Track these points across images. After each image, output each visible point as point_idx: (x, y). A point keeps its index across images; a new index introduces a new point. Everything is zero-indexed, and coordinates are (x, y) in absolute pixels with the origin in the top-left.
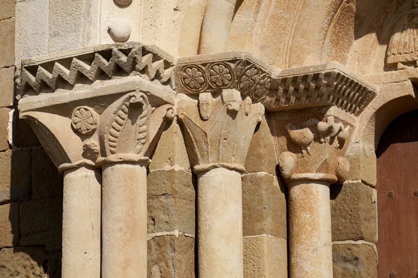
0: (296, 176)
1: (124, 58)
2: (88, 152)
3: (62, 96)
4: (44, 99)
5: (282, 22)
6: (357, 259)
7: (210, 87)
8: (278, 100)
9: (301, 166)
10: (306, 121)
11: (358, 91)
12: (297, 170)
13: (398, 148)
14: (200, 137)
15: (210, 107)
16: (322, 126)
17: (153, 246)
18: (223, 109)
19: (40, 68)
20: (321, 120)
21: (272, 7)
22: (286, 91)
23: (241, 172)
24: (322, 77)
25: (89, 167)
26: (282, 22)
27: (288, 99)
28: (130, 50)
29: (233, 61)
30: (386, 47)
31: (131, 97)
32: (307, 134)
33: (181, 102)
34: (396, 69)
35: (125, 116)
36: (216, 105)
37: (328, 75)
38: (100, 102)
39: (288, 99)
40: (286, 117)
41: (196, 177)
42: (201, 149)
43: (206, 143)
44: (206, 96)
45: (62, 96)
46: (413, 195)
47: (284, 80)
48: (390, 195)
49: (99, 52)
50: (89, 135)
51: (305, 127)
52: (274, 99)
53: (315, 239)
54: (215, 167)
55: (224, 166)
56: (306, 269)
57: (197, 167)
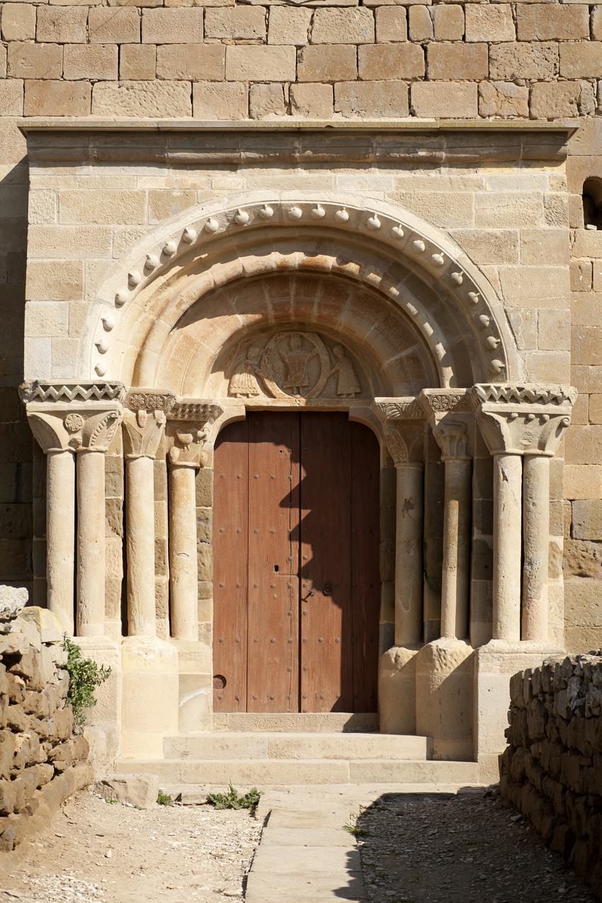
1: (111, 390)
2: (73, 443)
3: (61, 406)
4: (48, 405)
5: (179, 365)
6: (207, 519)
7: (147, 407)
8: (176, 415)
9: (182, 457)
10: (190, 429)
12: (179, 459)
13: (227, 445)
14: (137, 438)
15: (146, 419)
16: (200, 433)
18: (155, 422)
19: (51, 387)
20: (199, 430)
21: (173, 353)
22: (183, 411)
23: (153, 459)
24: (209, 407)
25: (70, 451)
26: (179, 365)
27: (183, 416)
28: (116, 386)
29: (166, 396)
30: (228, 381)
31: (112, 413)
32: (190, 437)
33: (126, 413)
34: (236, 397)
35: (105, 424)
36: (149, 418)
37: (213, 406)
38: (88, 413)
39: (183, 416)
40: (177, 425)
42: (136, 445)
43: (140, 441)
44: (142, 412)
45: (61, 406)
46: (236, 478)
47: (184, 405)
48: (221, 477)
49: (96, 385)
51: (189, 433)
52: (174, 414)
53: (189, 505)
54: (143, 456)
55: (147, 457)
56: (184, 525)
57: (130, 455)
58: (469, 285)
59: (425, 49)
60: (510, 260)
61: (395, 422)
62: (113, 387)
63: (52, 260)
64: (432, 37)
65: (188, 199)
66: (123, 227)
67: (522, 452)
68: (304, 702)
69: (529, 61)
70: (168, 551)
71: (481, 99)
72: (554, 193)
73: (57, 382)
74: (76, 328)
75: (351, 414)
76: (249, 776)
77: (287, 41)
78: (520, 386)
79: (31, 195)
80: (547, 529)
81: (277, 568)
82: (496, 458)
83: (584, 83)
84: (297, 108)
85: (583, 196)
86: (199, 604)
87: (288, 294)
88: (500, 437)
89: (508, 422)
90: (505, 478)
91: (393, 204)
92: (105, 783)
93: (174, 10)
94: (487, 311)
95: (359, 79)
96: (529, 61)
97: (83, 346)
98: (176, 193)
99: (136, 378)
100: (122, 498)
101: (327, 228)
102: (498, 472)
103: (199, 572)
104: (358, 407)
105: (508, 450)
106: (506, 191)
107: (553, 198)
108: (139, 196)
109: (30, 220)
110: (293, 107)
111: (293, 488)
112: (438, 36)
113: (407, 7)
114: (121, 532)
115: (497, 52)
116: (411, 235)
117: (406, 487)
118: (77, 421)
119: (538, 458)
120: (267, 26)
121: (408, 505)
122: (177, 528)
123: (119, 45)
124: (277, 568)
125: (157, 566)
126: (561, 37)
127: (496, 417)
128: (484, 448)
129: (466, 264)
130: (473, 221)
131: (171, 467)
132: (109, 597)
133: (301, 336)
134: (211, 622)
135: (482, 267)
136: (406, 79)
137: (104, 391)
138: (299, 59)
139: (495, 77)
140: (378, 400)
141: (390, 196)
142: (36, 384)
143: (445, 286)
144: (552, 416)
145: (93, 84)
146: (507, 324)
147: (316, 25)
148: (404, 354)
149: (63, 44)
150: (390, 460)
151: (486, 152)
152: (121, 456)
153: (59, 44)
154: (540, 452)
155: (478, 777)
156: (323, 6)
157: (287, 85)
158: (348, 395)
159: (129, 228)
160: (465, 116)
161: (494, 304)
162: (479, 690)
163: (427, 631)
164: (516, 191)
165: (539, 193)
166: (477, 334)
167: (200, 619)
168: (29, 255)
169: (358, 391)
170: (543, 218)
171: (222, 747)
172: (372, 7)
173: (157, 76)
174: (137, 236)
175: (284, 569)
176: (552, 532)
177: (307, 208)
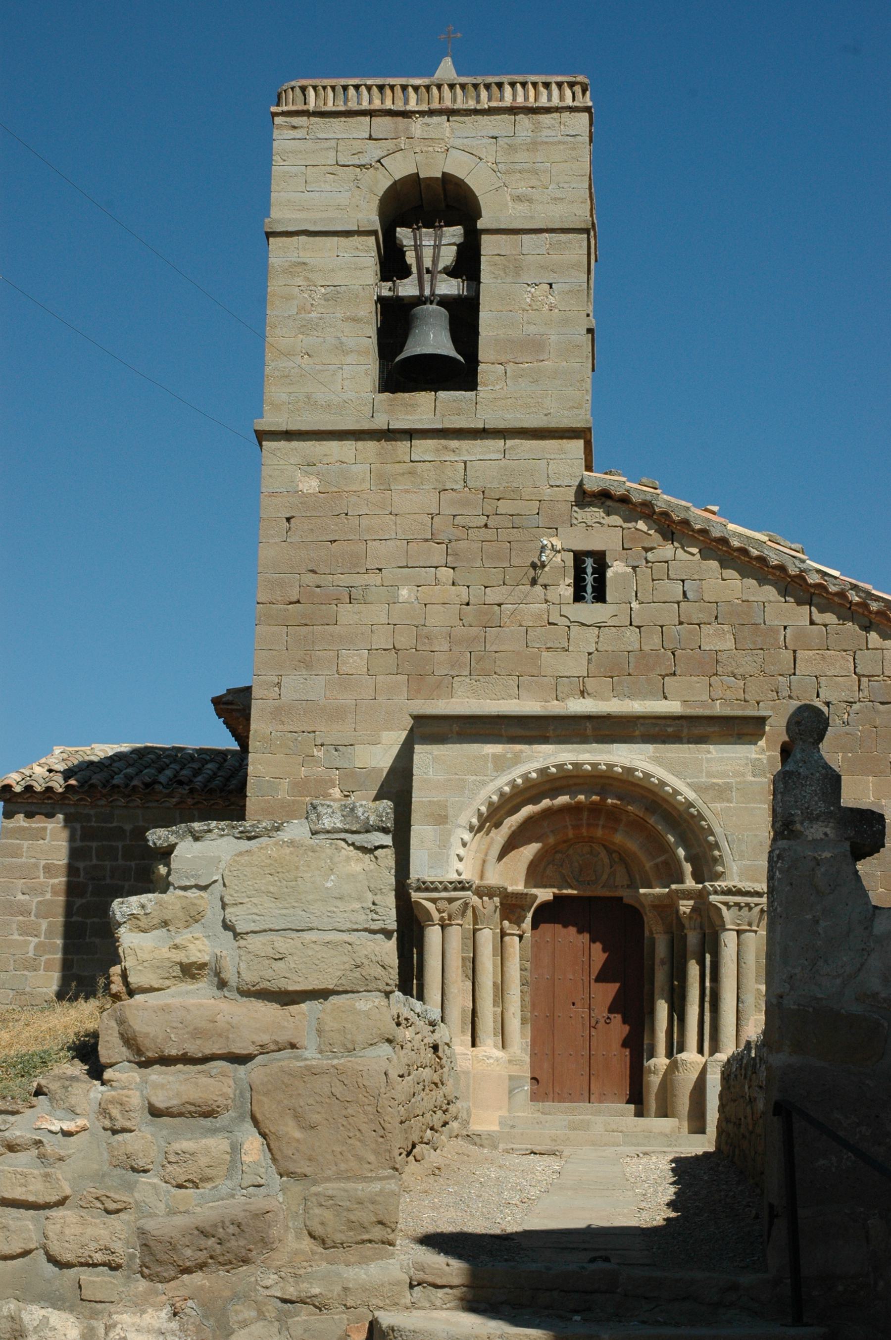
0: (508, 931)
1: (467, 885)
2: (442, 919)
11: (667, 1084)
13: (543, 927)
17: (642, 855)
25: (438, 924)
38: (451, 900)
41: (475, 931)
42: (481, 920)
50: (443, 912)
57: (477, 927)
58: (701, 817)
59: (674, 655)
60: (729, 801)
61: (655, 907)
62: (468, 883)
63: (428, 799)
64: (678, 647)
65: (517, 760)
66: (474, 777)
67: (737, 928)
68: (592, 1097)
69: (744, 663)
70: (501, 991)
71: (711, 688)
72: (758, 756)
73: (431, 879)
74: (444, 844)
75: (624, 900)
76: (555, 1141)
77: (582, 649)
78: (735, 884)
79: (415, 757)
80: (754, 980)
81: (574, 1004)
82: (719, 932)
83: (780, 678)
84: (588, 694)
85: (781, 753)
86: (521, 1028)
87: (582, 819)
88: (722, 917)
89: (728, 910)
90: (726, 945)
91: (651, 763)
92: (468, 1136)
93: (507, 629)
94: (713, 834)
95: (630, 675)
96: (744, 663)
97: (448, 856)
98: (509, 756)
99: (482, 877)
100: (472, 955)
101: (608, 777)
102: (720, 941)
103: (522, 1006)
104: (756, 779)
105: (728, 927)
106: (725, 755)
107: (756, 759)
108: (485, 757)
109: (415, 772)
110: (585, 694)
111: (267, 344)
112: (683, 647)
113: (662, 627)
114: (471, 978)
115: (722, 657)
116: (663, 784)
117: (661, 950)
118: (442, 904)
119: (747, 933)
120: (569, 639)
121: (663, 963)
122: (507, 975)
123: (470, 652)
124: (574, 1004)
125: (494, 1001)
126: (764, 647)
127: (719, 905)
128: (712, 925)
129: (699, 803)
130: (704, 774)
131: (503, 934)
132: (463, 1022)
133: (591, 846)
134: (529, 1040)
135: (709, 805)
136: (661, 675)
137: (461, 886)
138: (589, 661)
139: (721, 674)
140: (642, 891)
141: (649, 758)
142: (418, 880)
143: (686, 816)
144: (756, 905)
145: (453, 678)
146: (726, 843)
147: (601, 639)
148: (660, 860)
149: (433, 652)
150: (651, 932)
151: (712, 730)
152: (472, 927)
153: (432, 652)
154: (748, 928)
155: (707, 1144)
156: (605, 626)
157: (581, 678)
158: (622, 886)
159: (478, 778)
160: (701, 699)
161: (717, 830)
162: (708, 1086)
163: (675, 1047)
164: (732, 755)
165: (747, 757)
166: (707, 850)
167: (522, 1038)
168: (413, 795)
169: (629, 883)
170: (750, 773)
171: (537, 1123)
172: (639, 627)
173: (495, 673)
174: (484, 784)
175: (579, 1004)
176: (757, 982)
177: (594, 765)
